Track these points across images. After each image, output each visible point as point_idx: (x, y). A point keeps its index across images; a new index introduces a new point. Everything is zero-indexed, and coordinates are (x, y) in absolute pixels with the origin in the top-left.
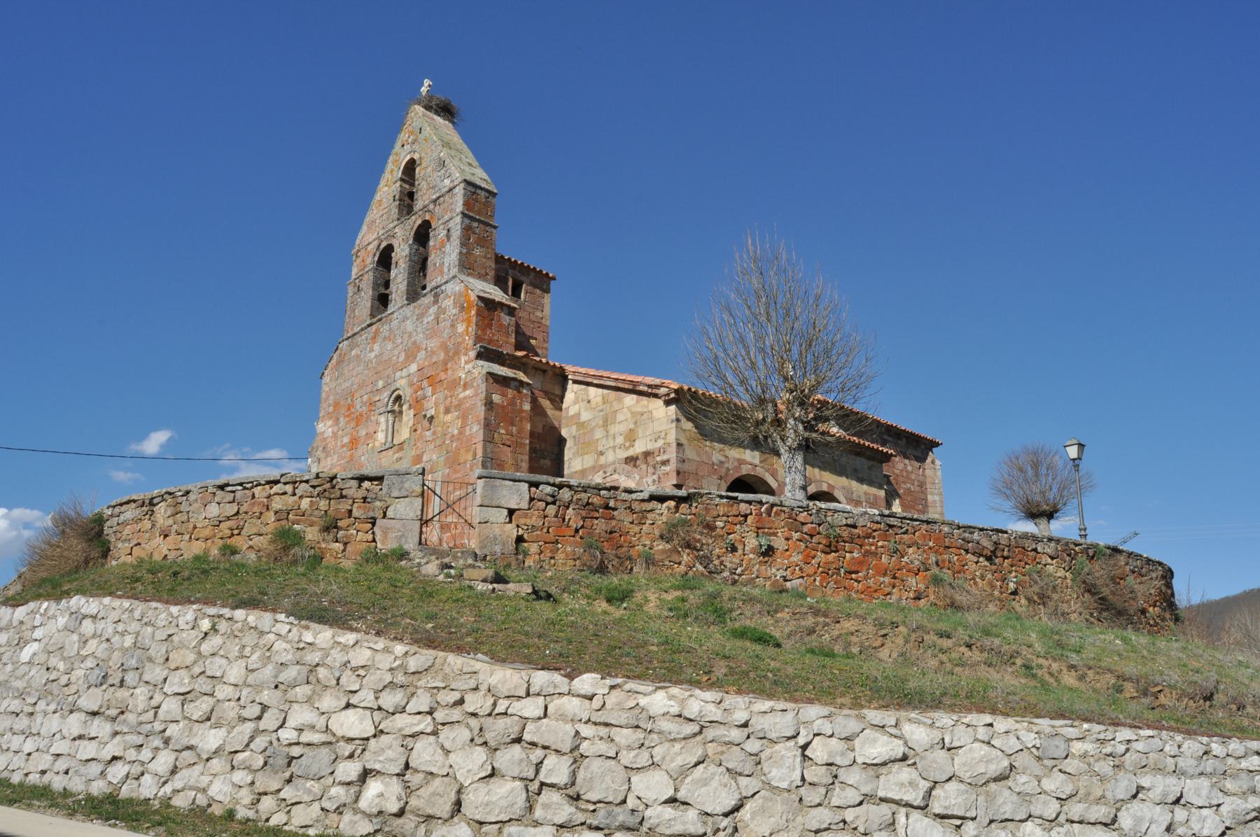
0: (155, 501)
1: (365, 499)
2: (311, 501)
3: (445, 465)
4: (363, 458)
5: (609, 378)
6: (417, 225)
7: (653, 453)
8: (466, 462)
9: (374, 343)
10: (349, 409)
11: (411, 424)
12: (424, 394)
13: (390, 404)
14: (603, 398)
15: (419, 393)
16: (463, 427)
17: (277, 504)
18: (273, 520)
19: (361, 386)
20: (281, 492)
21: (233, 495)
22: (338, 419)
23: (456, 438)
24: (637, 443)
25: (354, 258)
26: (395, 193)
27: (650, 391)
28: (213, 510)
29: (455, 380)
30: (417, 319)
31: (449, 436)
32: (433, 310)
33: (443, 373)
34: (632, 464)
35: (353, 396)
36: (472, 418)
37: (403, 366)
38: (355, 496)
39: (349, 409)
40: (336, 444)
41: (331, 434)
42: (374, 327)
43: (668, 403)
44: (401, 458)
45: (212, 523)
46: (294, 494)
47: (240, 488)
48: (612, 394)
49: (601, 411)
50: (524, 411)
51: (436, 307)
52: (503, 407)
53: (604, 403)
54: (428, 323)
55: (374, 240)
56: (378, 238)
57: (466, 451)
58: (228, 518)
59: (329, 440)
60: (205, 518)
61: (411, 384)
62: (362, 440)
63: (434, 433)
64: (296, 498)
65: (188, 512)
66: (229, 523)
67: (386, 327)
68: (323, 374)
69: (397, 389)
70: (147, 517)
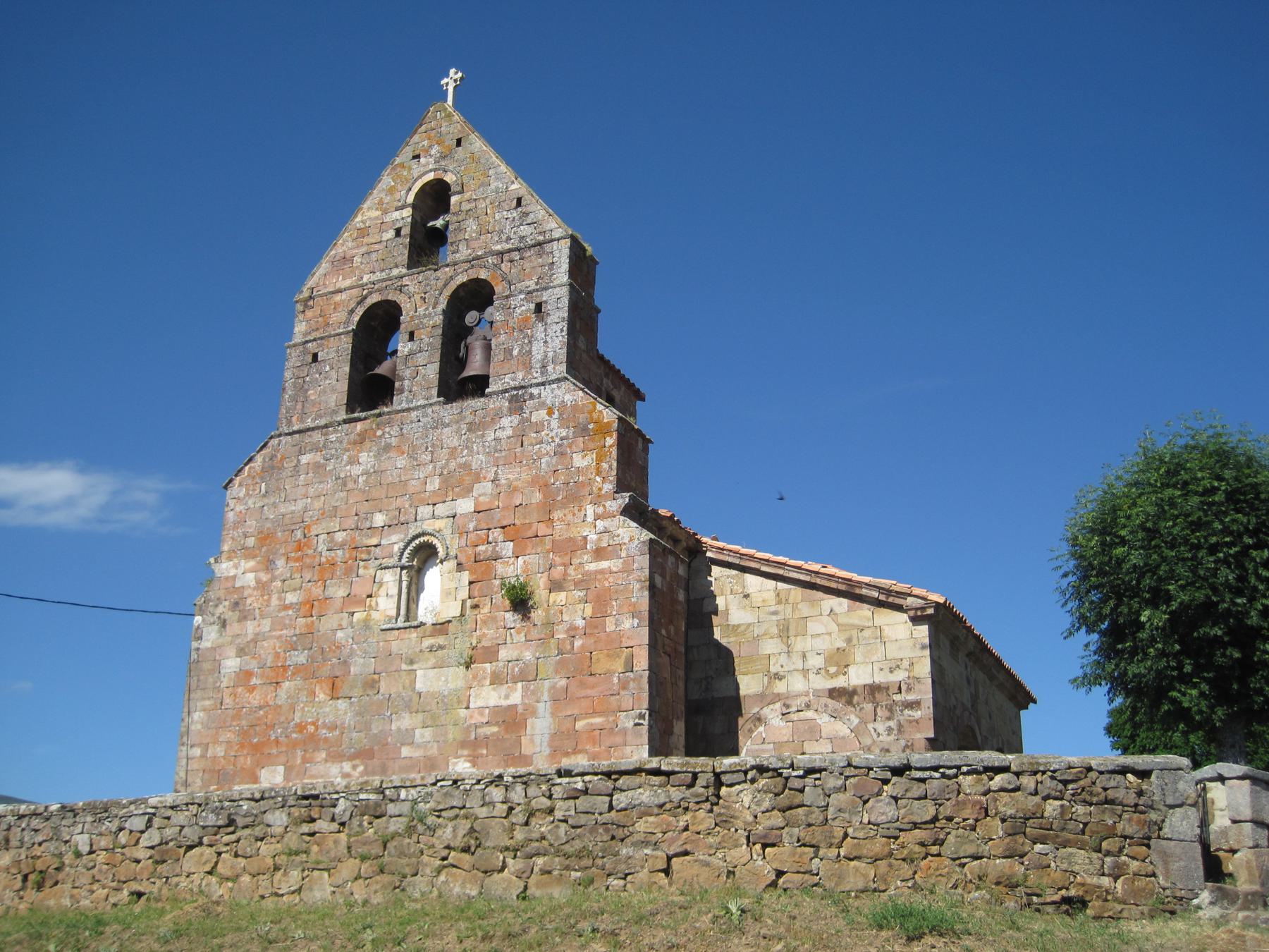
5: (799, 568)
6: (458, 282)
7: (887, 688)
8: (609, 673)
13: (406, 555)
14: (778, 595)
17: (1007, 806)
20: (1011, 787)
24: (852, 670)
25: (300, 307)
27: (882, 598)
28: (882, 810)
32: (508, 423)
34: (844, 699)
36: (620, 606)
39: (299, 549)
43: (916, 620)
44: (441, 647)
46: (1036, 793)
48: (796, 592)
49: (775, 613)
53: (779, 602)
64: (1037, 799)
66: (918, 834)
67: (395, 430)
68: (231, 481)
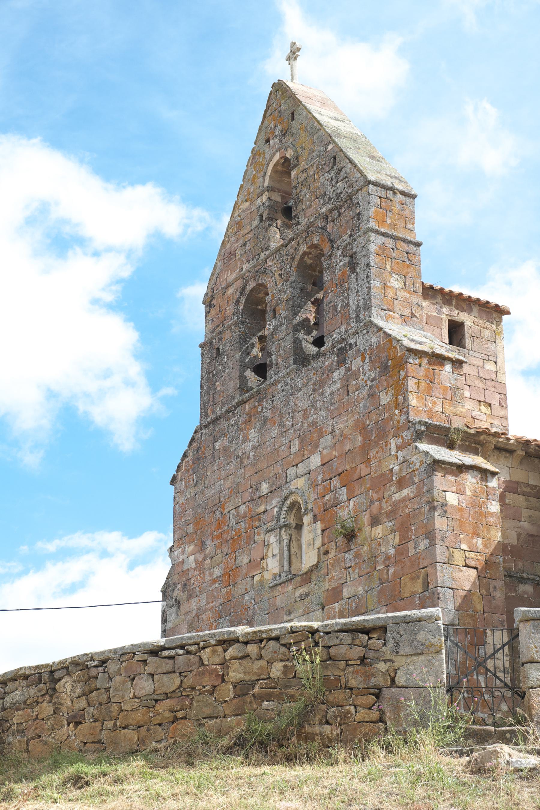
0: (57, 675)
1: (363, 659)
2: (285, 667)
3: (379, 602)
4: (247, 597)
9: (249, 429)
10: (219, 527)
11: (318, 543)
12: (335, 498)
15: (327, 497)
16: (404, 541)
18: (232, 696)
19: (235, 491)
21: (171, 662)
22: (203, 543)
23: (393, 560)
26: (261, 211)
29: (383, 474)
30: (314, 390)
31: (380, 559)
33: (363, 466)
35: (223, 507)
36: (417, 529)
37: (299, 460)
38: (347, 656)
39: (219, 527)
40: (203, 578)
41: (193, 565)
42: (248, 406)
44: (307, 595)
45: (144, 703)
46: (260, 658)
47: (181, 652)
50: (491, 514)
51: (342, 370)
52: (461, 510)
54: (332, 394)
55: (236, 280)
56: (242, 277)
57: (412, 579)
58: (167, 696)
59: (191, 573)
60: (135, 697)
61: (313, 485)
62: (244, 569)
63: (357, 556)
64: (263, 663)
65: (108, 690)
69: (291, 494)
70: (47, 698)
